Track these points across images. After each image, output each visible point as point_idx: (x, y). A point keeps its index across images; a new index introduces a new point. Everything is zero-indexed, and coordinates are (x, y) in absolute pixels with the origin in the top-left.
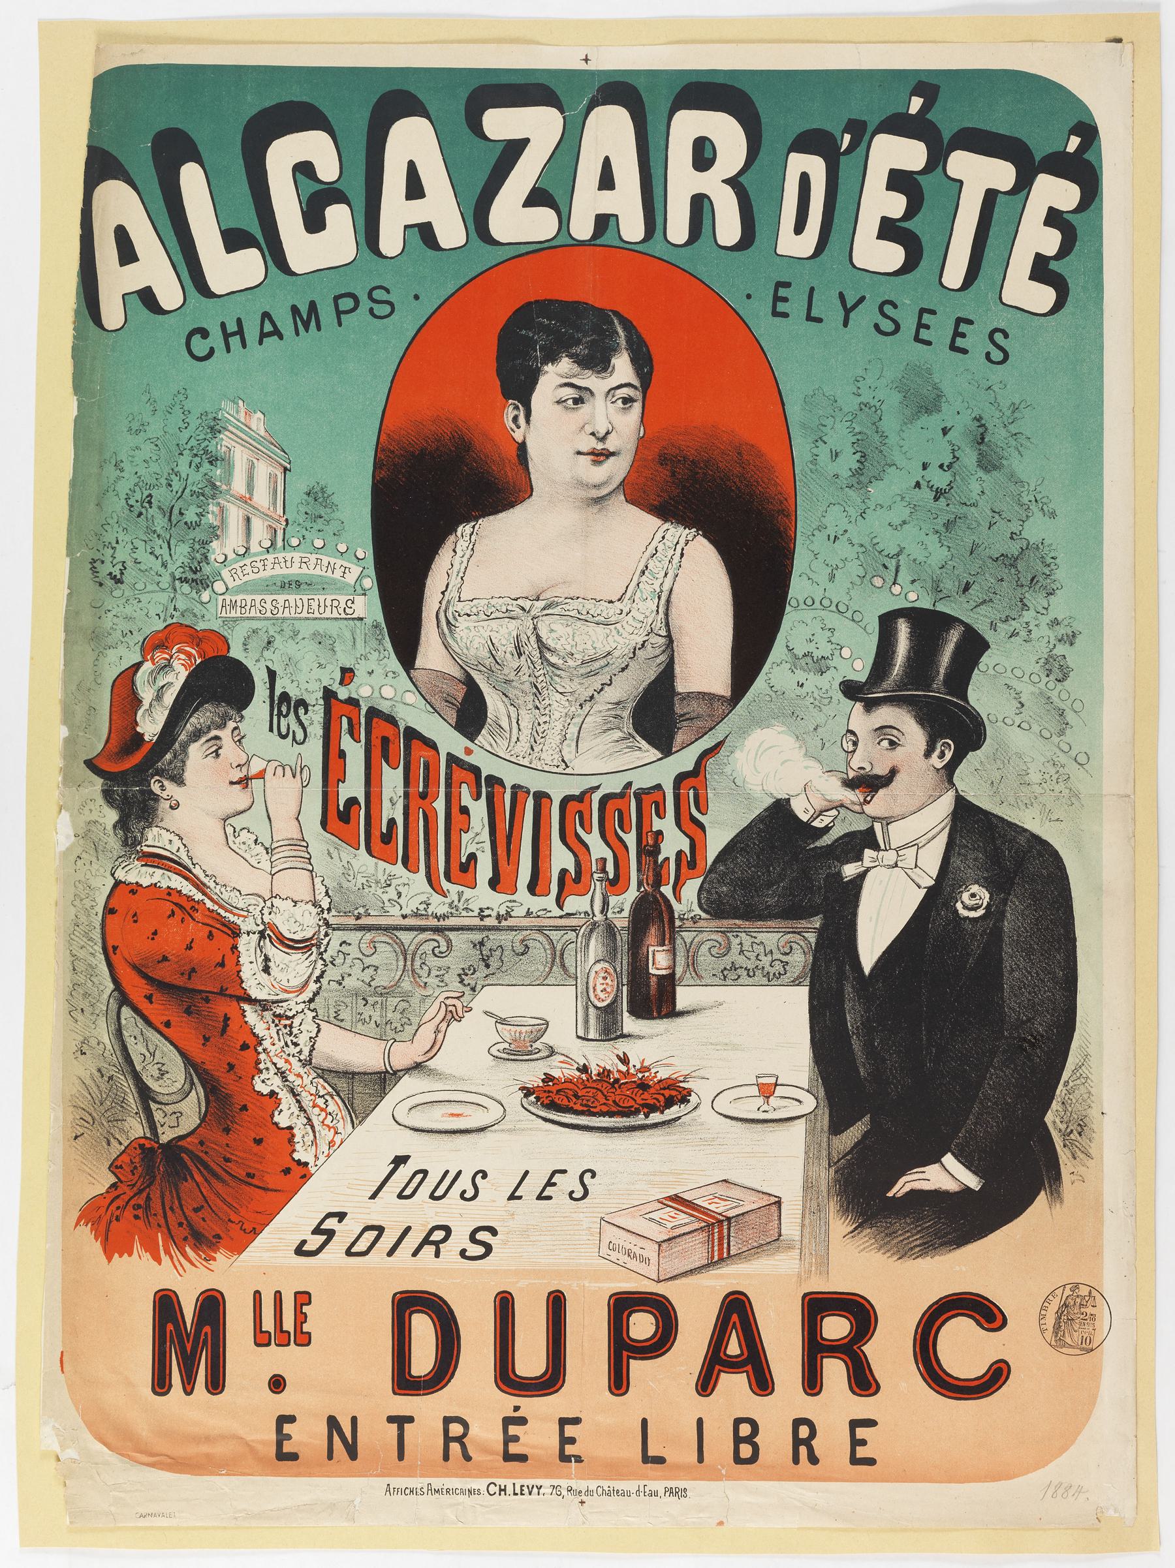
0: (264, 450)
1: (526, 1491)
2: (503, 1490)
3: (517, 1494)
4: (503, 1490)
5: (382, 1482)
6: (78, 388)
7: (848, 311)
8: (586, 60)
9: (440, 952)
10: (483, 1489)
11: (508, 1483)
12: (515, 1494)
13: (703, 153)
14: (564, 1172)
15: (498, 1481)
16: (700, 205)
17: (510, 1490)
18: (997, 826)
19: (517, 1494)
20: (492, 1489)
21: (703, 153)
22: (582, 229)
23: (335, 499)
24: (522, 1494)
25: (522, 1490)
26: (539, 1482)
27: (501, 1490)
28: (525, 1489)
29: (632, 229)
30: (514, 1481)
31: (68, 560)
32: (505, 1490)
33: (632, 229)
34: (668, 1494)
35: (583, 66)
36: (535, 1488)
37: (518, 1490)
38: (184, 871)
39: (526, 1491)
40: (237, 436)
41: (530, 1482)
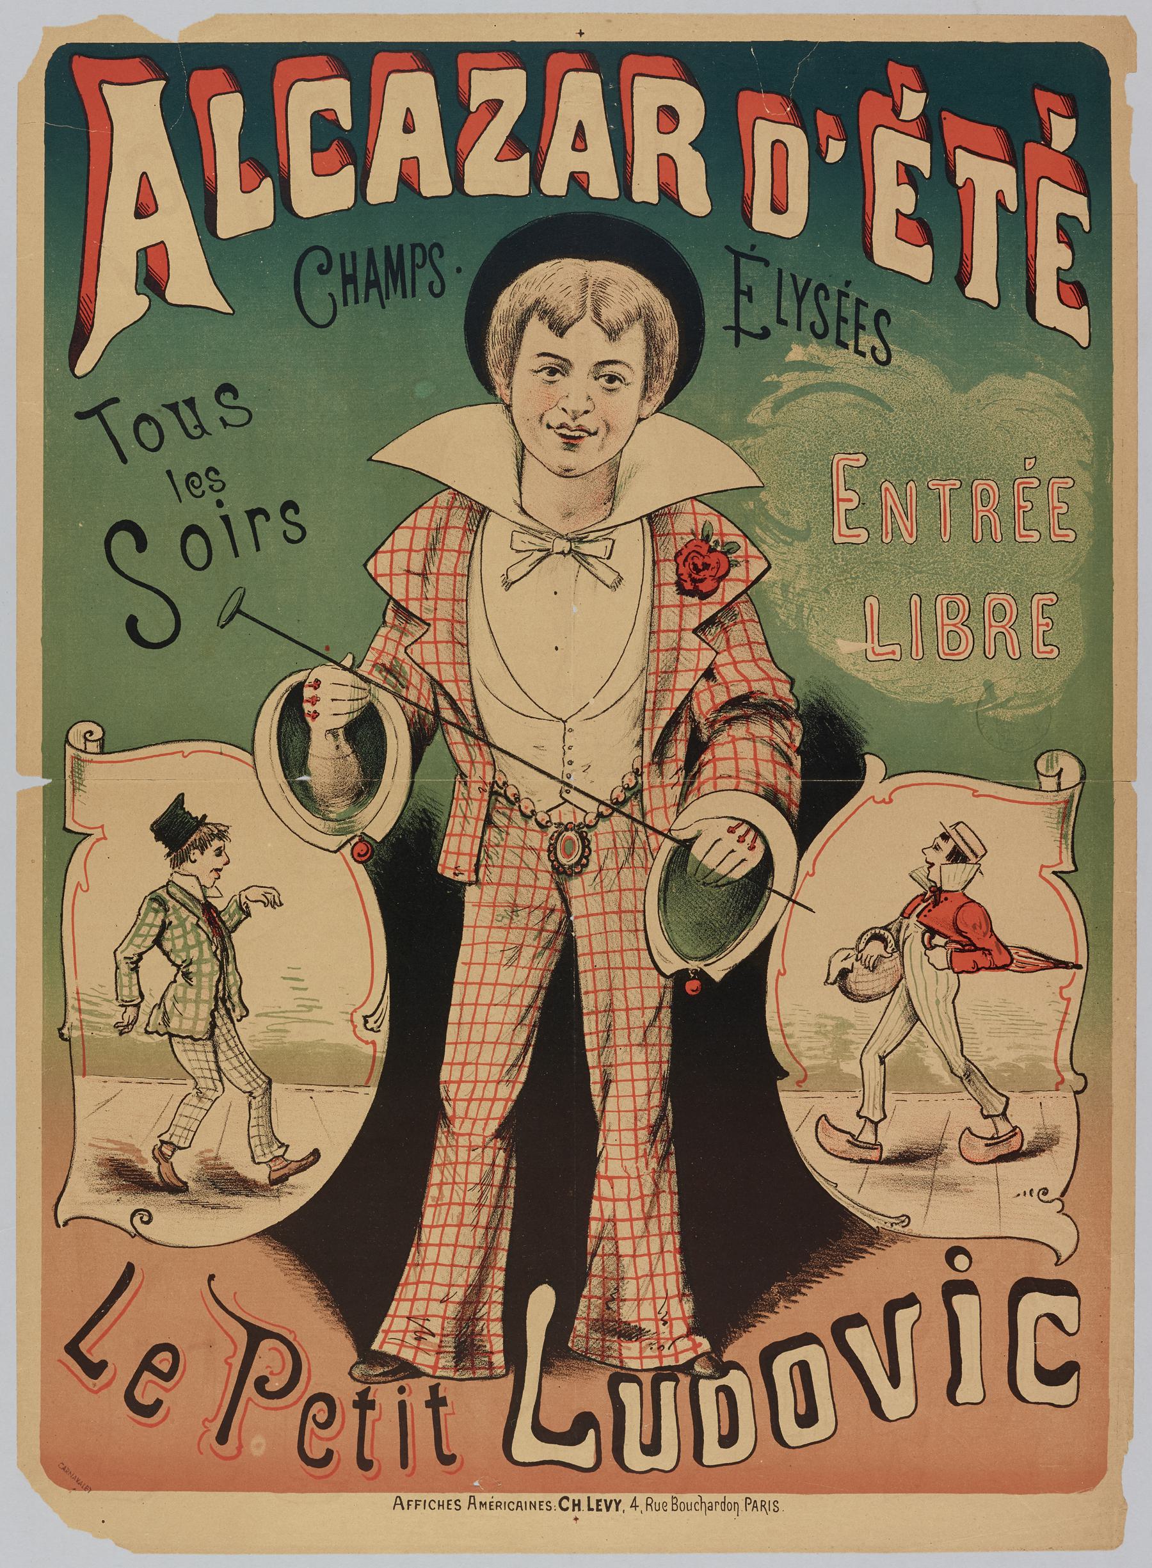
0: (914, 643)
1: (603, 1506)
2: (577, 1505)
3: (592, 1510)
4: (577, 1505)
7: (738, 255)
8: (581, 34)
10: (555, 1503)
11: (583, 1497)
12: (590, 1509)
13: (668, 116)
15: (572, 1496)
16: (666, 162)
20: (565, 1504)
21: (668, 116)
22: (554, 183)
23: (566, 521)
24: (598, 1510)
25: (598, 1505)
27: (574, 1505)
28: (602, 1504)
29: (604, 186)
30: (589, 1495)
31: (95, 17)
32: (579, 1505)
33: (604, 186)
34: (750, 1507)
35: (578, 39)
36: (613, 1502)
37: (593, 1505)
39: (603, 1506)
40: (872, 627)
41: (609, 1497)
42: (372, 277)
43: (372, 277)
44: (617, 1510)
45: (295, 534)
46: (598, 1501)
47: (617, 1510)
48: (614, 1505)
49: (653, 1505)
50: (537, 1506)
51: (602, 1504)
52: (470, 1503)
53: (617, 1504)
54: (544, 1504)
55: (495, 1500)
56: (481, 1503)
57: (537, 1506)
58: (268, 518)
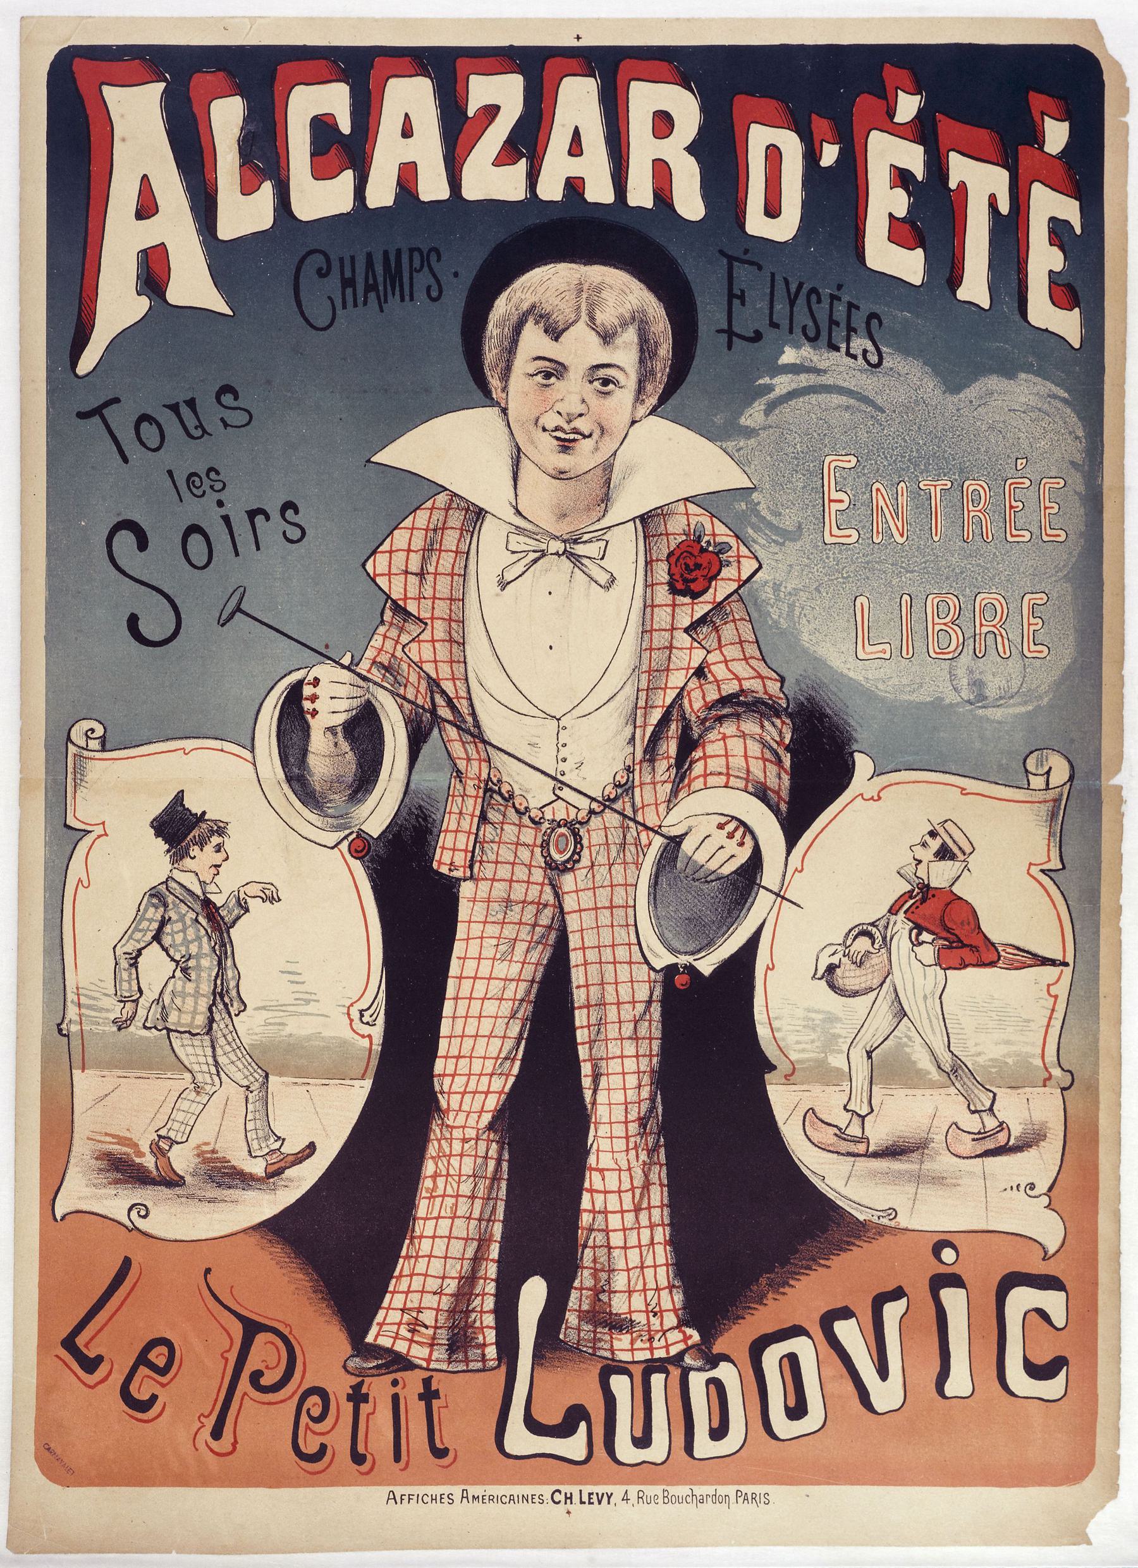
1: (594, 1499)
4: (569, 1498)
5: (384, 1490)
6: (1123, 677)
7: (731, 259)
8: (578, 38)
9: (194, 481)
11: (574, 1490)
12: (582, 1502)
13: (663, 123)
14: (116, 400)
17: (576, 1498)
18: (808, 648)
19: (584, 1503)
20: (557, 1497)
21: (663, 123)
24: (590, 1503)
25: (590, 1499)
26: (608, 1489)
27: (566, 1498)
28: (594, 1497)
30: (581, 1487)
32: (571, 1498)
34: (741, 1500)
35: (575, 43)
37: (585, 1498)
38: (469, 1280)
39: (594, 1499)
42: (371, 282)
43: (371, 282)
44: (609, 1503)
45: (294, 533)
46: (590, 1494)
47: (609, 1503)
48: (605, 1498)
49: (644, 1498)
50: (438, 1498)
51: (594, 1497)
52: (463, 1497)
53: (609, 1498)
54: (537, 1497)
55: (488, 1493)
56: (474, 1496)
57: (438, 1498)
58: (268, 518)
